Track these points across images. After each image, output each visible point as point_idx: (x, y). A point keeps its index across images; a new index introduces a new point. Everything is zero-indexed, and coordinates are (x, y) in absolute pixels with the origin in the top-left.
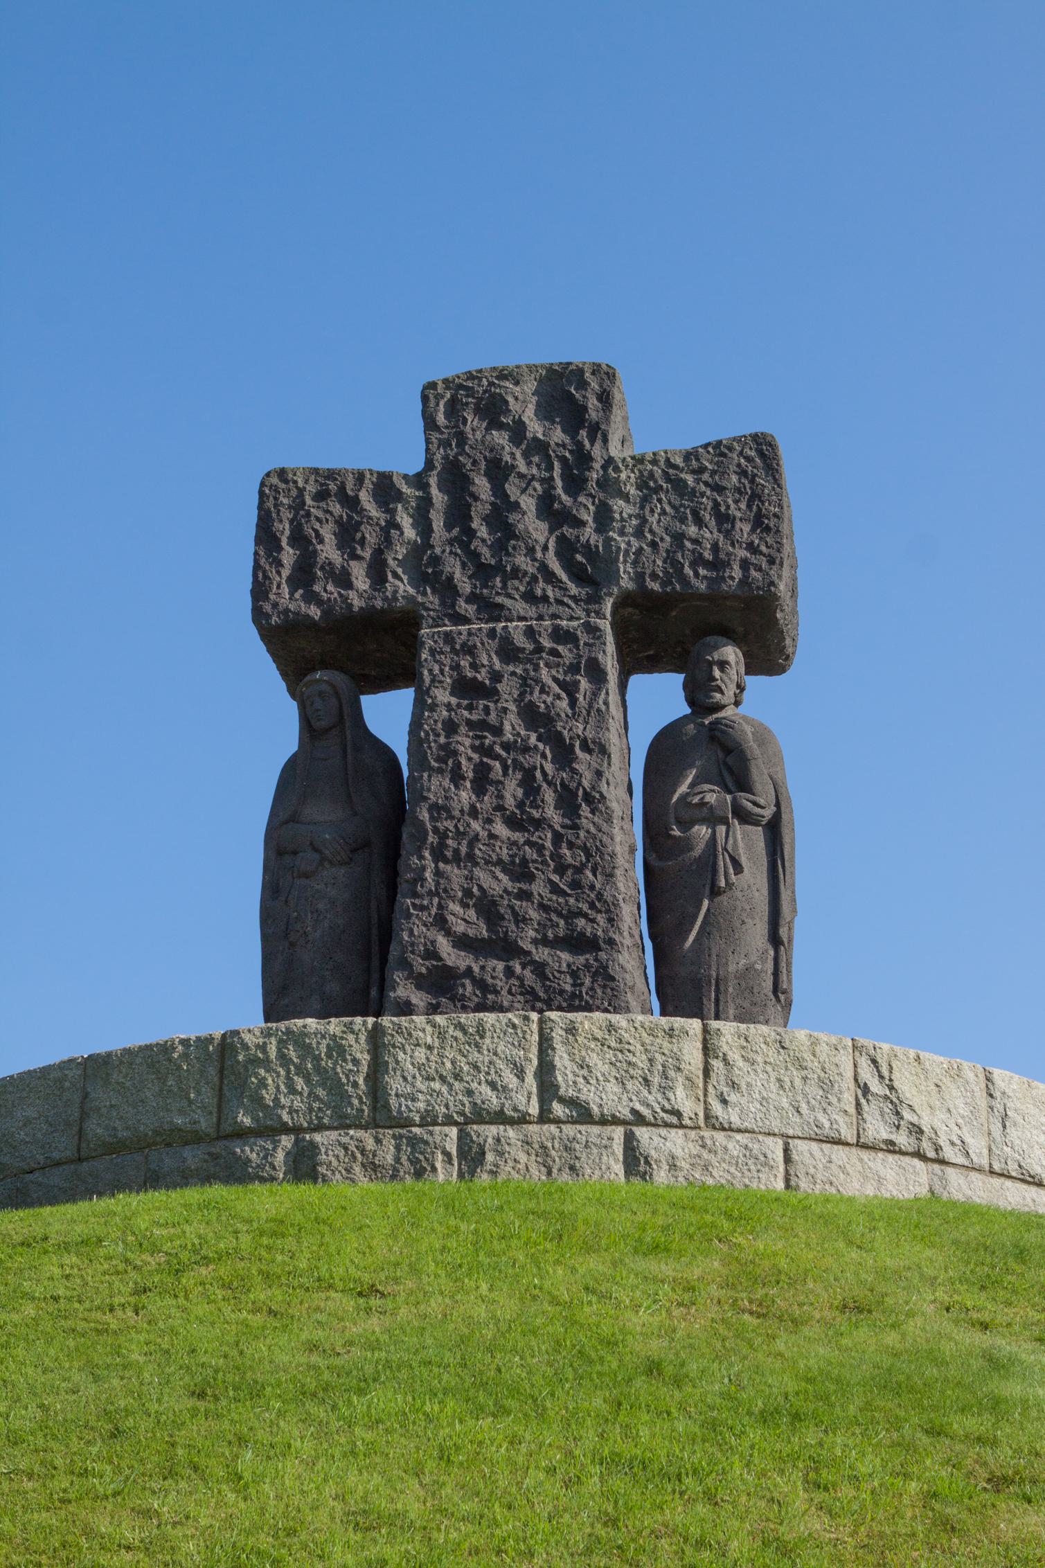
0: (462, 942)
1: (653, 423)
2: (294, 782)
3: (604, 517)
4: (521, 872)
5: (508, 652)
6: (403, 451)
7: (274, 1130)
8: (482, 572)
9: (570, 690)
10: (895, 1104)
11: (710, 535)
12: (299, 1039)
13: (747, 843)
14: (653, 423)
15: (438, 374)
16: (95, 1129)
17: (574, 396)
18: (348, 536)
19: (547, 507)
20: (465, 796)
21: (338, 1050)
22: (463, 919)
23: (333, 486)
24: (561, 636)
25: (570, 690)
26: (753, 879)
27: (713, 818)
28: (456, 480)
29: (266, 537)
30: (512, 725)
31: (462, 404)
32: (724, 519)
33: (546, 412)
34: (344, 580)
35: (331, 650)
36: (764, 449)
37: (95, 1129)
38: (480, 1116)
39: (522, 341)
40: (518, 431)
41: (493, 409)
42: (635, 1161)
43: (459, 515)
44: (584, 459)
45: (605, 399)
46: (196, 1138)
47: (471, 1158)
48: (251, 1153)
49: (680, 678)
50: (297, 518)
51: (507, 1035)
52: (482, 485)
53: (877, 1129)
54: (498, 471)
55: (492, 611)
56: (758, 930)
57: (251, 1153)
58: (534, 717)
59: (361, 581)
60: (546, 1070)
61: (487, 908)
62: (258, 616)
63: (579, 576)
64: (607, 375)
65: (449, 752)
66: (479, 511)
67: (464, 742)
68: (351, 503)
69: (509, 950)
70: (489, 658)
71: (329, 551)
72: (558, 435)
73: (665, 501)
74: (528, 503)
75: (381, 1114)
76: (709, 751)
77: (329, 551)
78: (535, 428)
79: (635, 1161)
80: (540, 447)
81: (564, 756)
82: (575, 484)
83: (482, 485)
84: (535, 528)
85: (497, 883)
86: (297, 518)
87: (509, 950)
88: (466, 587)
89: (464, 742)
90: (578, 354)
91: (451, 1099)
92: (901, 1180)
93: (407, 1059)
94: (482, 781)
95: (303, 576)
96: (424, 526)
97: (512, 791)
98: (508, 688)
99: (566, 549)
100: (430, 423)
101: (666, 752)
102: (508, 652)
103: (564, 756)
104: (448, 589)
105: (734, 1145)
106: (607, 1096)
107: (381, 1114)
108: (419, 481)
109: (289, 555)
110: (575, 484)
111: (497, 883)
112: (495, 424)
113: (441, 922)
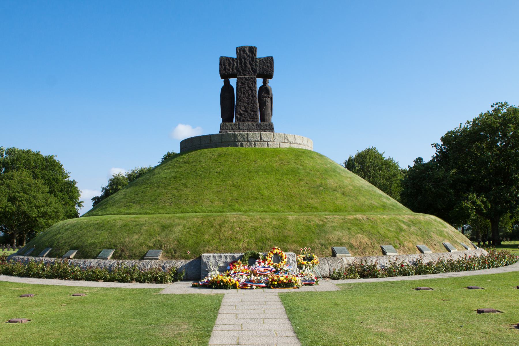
0: (243, 111)
1: (260, 54)
2: (223, 89)
3: (256, 65)
4: (248, 104)
5: (246, 80)
6: (235, 56)
7: (239, 141)
8: (243, 70)
9: (252, 84)
10: (287, 139)
11: (266, 68)
12: (241, 134)
13: (269, 100)
14: (260, 54)
15: (238, 46)
16: (223, 140)
17: (252, 50)
18: (229, 65)
19: (250, 63)
20: (242, 95)
21: (244, 135)
22: (243, 108)
23: (227, 59)
24: (251, 78)
25: (252, 84)
26: (269, 104)
27: (266, 97)
28: (240, 59)
29: (220, 64)
30: (247, 88)
31: (240, 50)
32: (268, 66)
33: (249, 52)
34: (229, 70)
35: (225, 75)
36: (272, 58)
37: (223, 140)
38: (256, 141)
39: (247, 43)
40: (247, 54)
41: (244, 51)
42: (268, 145)
43: (241, 63)
44: (254, 58)
45: (256, 51)
46: (232, 142)
47: (255, 144)
48: (237, 143)
49: (263, 79)
50: (224, 62)
51: (257, 134)
52: (243, 60)
53: (286, 141)
54: (245, 59)
55: (245, 75)
56: (270, 109)
57: (237, 143)
58: (249, 87)
59: (231, 70)
60: (261, 137)
61: (245, 107)
62: (220, 73)
63: (253, 71)
64: (256, 48)
65: (241, 91)
66: (243, 63)
67: (242, 89)
68: (230, 61)
69: (247, 112)
70: (244, 80)
71: (227, 67)
72: (251, 55)
73: (262, 64)
74: (248, 63)
75: (248, 141)
76: (265, 90)
77: (227, 67)
78: (248, 54)
79: (268, 145)
80: (249, 56)
81: (252, 91)
82: (253, 61)
83: (243, 60)
84: (249, 66)
85: (246, 105)
86: (224, 62)
87: (247, 112)
88: (242, 71)
89: (242, 89)
90: (253, 45)
91: (253, 140)
92: (287, 146)
93: (250, 136)
94: (244, 94)
95: (225, 69)
96: (237, 64)
97: (247, 95)
98: (246, 84)
99: (252, 68)
100: (237, 52)
101: (261, 88)
102: (246, 80)
103: (252, 91)
104: (240, 72)
105: (275, 143)
106: (266, 139)
107: (248, 141)
108: (236, 59)
109: (223, 67)
110: (253, 61)
111: (246, 105)
112: (244, 53)
113: (241, 108)
